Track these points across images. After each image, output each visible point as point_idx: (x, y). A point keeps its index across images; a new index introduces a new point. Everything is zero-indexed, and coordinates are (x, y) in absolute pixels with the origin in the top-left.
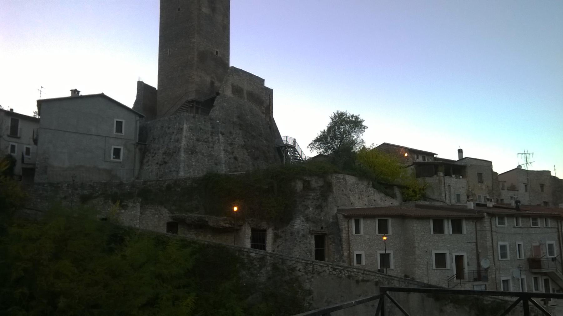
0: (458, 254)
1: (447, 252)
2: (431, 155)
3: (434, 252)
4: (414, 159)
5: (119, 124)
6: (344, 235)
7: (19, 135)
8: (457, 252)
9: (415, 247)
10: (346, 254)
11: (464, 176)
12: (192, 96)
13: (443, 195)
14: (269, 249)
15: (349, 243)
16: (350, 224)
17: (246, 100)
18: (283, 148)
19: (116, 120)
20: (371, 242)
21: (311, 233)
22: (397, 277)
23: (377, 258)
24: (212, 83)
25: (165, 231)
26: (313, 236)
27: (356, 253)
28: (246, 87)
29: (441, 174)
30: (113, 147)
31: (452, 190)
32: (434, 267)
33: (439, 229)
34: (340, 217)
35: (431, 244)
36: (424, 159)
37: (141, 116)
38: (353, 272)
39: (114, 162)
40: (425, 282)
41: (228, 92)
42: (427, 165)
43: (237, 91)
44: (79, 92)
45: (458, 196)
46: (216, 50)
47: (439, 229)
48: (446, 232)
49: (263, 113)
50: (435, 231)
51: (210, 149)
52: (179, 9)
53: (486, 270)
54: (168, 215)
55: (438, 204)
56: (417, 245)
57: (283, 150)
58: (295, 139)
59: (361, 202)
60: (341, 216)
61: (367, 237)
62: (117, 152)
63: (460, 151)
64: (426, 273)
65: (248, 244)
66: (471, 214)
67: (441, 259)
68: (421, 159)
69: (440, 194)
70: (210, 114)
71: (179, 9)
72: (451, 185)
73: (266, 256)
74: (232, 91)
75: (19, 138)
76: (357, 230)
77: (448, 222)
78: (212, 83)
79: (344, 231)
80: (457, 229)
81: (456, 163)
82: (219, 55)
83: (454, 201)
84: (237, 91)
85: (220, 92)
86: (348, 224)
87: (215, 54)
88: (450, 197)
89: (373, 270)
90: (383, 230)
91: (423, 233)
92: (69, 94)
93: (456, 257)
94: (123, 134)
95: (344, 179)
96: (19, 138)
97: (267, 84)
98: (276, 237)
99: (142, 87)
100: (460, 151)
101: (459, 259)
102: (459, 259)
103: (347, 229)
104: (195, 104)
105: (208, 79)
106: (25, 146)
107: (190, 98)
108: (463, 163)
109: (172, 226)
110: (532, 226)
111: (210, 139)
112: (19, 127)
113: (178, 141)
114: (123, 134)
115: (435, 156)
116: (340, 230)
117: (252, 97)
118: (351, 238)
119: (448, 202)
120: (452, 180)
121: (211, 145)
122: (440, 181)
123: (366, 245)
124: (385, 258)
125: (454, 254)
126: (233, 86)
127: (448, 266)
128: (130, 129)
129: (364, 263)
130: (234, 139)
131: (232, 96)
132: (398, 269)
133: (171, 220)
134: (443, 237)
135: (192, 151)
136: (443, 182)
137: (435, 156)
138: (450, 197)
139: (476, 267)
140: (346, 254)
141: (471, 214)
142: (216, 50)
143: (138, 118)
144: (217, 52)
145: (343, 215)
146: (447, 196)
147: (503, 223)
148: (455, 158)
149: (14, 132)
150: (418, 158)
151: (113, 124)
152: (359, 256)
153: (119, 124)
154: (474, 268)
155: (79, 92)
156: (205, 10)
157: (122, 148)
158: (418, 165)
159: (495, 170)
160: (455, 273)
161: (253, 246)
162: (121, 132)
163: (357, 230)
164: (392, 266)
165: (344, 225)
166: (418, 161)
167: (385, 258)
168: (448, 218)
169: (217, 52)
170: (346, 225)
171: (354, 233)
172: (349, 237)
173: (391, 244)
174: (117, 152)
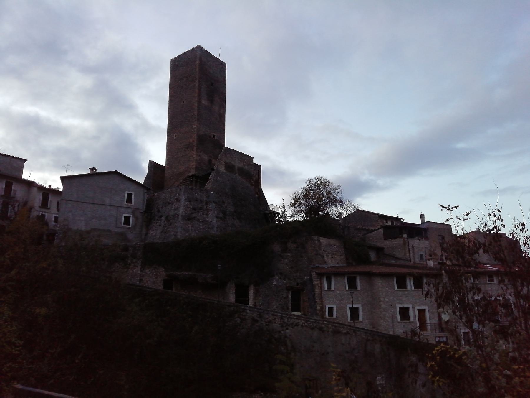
0: (420, 308)
1: (410, 306)
2: (398, 219)
3: (398, 306)
4: (383, 223)
5: (130, 196)
6: (317, 291)
7: (49, 207)
8: (419, 306)
9: (380, 301)
10: (319, 308)
11: (427, 238)
12: (192, 172)
13: (408, 255)
14: (251, 303)
15: (321, 298)
16: (322, 281)
17: (237, 175)
18: (270, 215)
19: (127, 192)
20: (341, 297)
21: (288, 289)
22: (364, 329)
23: (347, 311)
24: (210, 161)
25: (161, 288)
26: (290, 292)
27: (327, 306)
28: (238, 164)
29: (405, 236)
30: (124, 215)
31: (416, 250)
32: (399, 320)
33: (402, 285)
34: (314, 274)
35: (395, 299)
36: (392, 223)
37: (148, 189)
38: (324, 324)
39: (124, 228)
40: (391, 333)
41: (222, 169)
42: (394, 227)
43: (230, 168)
44: (96, 170)
45: (421, 255)
46: (214, 134)
47: (402, 285)
48: (409, 287)
49: (252, 185)
50: (349, 287)
51: (205, 216)
52: (183, 102)
53: (447, 322)
54: (164, 273)
55: (402, 262)
56: (382, 299)
57: (267, 215)
58: (423, 215)
59: (334, 261)
60: (314, 273)
61: (338, 292)
62: (127, 219)
63: (422, 216)
64: (391, 325)
65: (232, 298)
66: (431, 272)
67: (404, 313)
68: (389, 223)
69: (405, 254)
70: (206, 186)
71: (183, 102)
72: (415, 245)
73: (246, 309)
74: (225, 167)
75: (49, 209)
76: (329, 287)
77: (410, 279)
78: (210, 161)
79: (317, 287)
80: (418, 285)
81: (418, 226)
82: (216, 138)
83: (417, 260)
84: (230, 168)
85: (215, 168)
86: (320, 281)
87: (213, 137)
88: (414, 257)
89: (341, 322)
90: (352, 285)
91: (387, 289)
92: (88, 172)
93: (419, 310)
94: (133, 204)
95: (318, 240)
96: (49, 209)
97: (255, 161)
98: (257, 293)
99: (153, 166)
100: (422, 216)
101: (421, 312)
102: (421, 312)
103: (319, 285)
104: (194, 178)
105: (206, 158)
106: (54, 215)
107: (191, 174)
108: (425, 226)
109: (167, 284)
110: (488, 282)
111: (205, 208)
112: (49, 199)
113: (177, 209)
114: (133, 204)
115: (402, 220)
116: (313, 287)
117: (243, 172)
118: (324, 293)
119: (412, 260)
120: (415, 242)
121: (206, 212)
122: (404, 244)
123: (336, 300)
124: (354, 312)
125: (417, 308)
126: (226, 163)
127: (412, 319)
128: (139, 200)
129: (335, 315)
130: (226, 207)
131: (224, 171)
132: (366, 321)
133: (166, 278)
134: (406, 293)
135: (188, 218)
136: (407, 244)
137: (402, 220)
138: (414, 257)
139: (437, 319)
140: (319, 308)
141: (431, 272)
142: (214, 134)
143: (146, 191)
144: (214, 136)
145: (316, 273)
146: (411, 255)
147: (493, 281)
148: (418, 222)
149: (45, 204)
150: (387, 222)
151: (124, 196)
152: (331, 309)
153: (130, 196)
154: (436, 320)
155: (96, 170)
156: (204, 102)
157: (131, 216)
158: (385, 228)
159: (454, 232)
160: (418, 325)
161: (236, 301)
162: (131, 203)
163: (329, 287)
164: (361, 319)
165: (316, 282)
166: (387, 225)
167: (354, 312)
168: (410, 275)
169: (214, 136)
170: (319, 282)
171: (326, 289)
172: (321, 291)
173: (360, 299)
174: (127, 219)
